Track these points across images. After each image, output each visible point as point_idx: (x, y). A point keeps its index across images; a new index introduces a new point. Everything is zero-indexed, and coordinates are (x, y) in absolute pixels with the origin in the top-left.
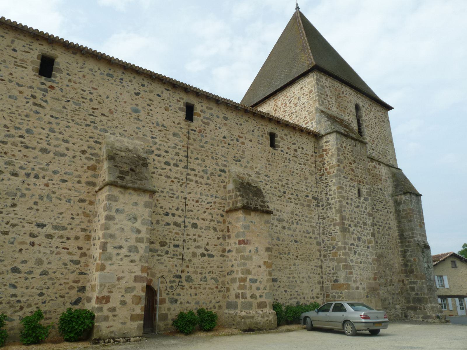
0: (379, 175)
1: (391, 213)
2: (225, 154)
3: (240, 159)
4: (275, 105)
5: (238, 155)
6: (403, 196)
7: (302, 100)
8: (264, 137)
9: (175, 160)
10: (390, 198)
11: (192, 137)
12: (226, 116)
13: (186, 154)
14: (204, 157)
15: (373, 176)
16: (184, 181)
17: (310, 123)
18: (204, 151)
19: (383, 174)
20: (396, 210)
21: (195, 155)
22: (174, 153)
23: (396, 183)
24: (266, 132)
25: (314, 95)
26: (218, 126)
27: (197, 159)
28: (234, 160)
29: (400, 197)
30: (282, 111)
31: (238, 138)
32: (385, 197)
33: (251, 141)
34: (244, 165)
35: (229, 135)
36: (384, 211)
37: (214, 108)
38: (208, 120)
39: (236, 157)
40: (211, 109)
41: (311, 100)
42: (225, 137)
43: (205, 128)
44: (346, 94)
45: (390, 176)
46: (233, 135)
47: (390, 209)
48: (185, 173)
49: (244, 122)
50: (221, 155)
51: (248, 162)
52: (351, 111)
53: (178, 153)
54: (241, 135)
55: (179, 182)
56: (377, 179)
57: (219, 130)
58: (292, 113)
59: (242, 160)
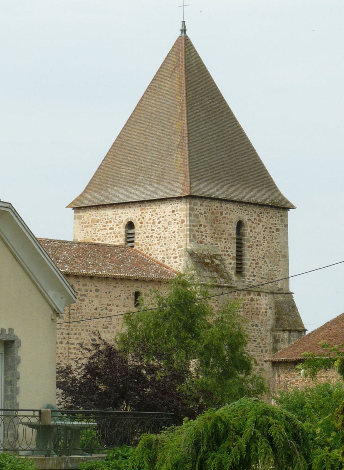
0: (257, 308)
1: (266, 352)
2: (96, 324)
3: (108, 326)
4: (141, 216)
5: (106, 323)
6: (282, 333)
7: (172, 227)
8: (130, 299)
9: (61, 339)
10: (268, 334)
11: (72, 316)
12: (97, 288)
13: (67, 332)
14: (80, 331)
15: (247, 312)
16: (67, 354)
17: (178, 258)
18: (81, 326)
19: (262, 306)
20: (273, 347)
21: (74, 331)
22: (60, 333)
23: (277, 316)
24: (131, 293)
25: (185, 228)
26: (91, 300)
27: (76, 334)
28: (103, 328)
29: (279, 333)
30: (149, 228)
31: (107, 306)
32: (262, 333)
33: (117, 306)
34: (111, 331)
35: (100, 306)
36: (258, 350)
37: (88, 284)
38: (84, 297)
39: (105, 325)
40: (86, 285)
41: (182, 232)
42: (96, 309)
43: (81, 305)
44: (226, 214)
45: (273, 305)
46: (102, 305)
47: (266, 347)
48: (67, 348)
49: (112, 289)
50: (93, 327)
51: (114, 327)
52: (230, 234)
53: (63, 332)
54: (110, 303)
55: (63, 356)
56: (253, 314)
57: (92, 304)
58: (160, 237)
59: (109, 326)
